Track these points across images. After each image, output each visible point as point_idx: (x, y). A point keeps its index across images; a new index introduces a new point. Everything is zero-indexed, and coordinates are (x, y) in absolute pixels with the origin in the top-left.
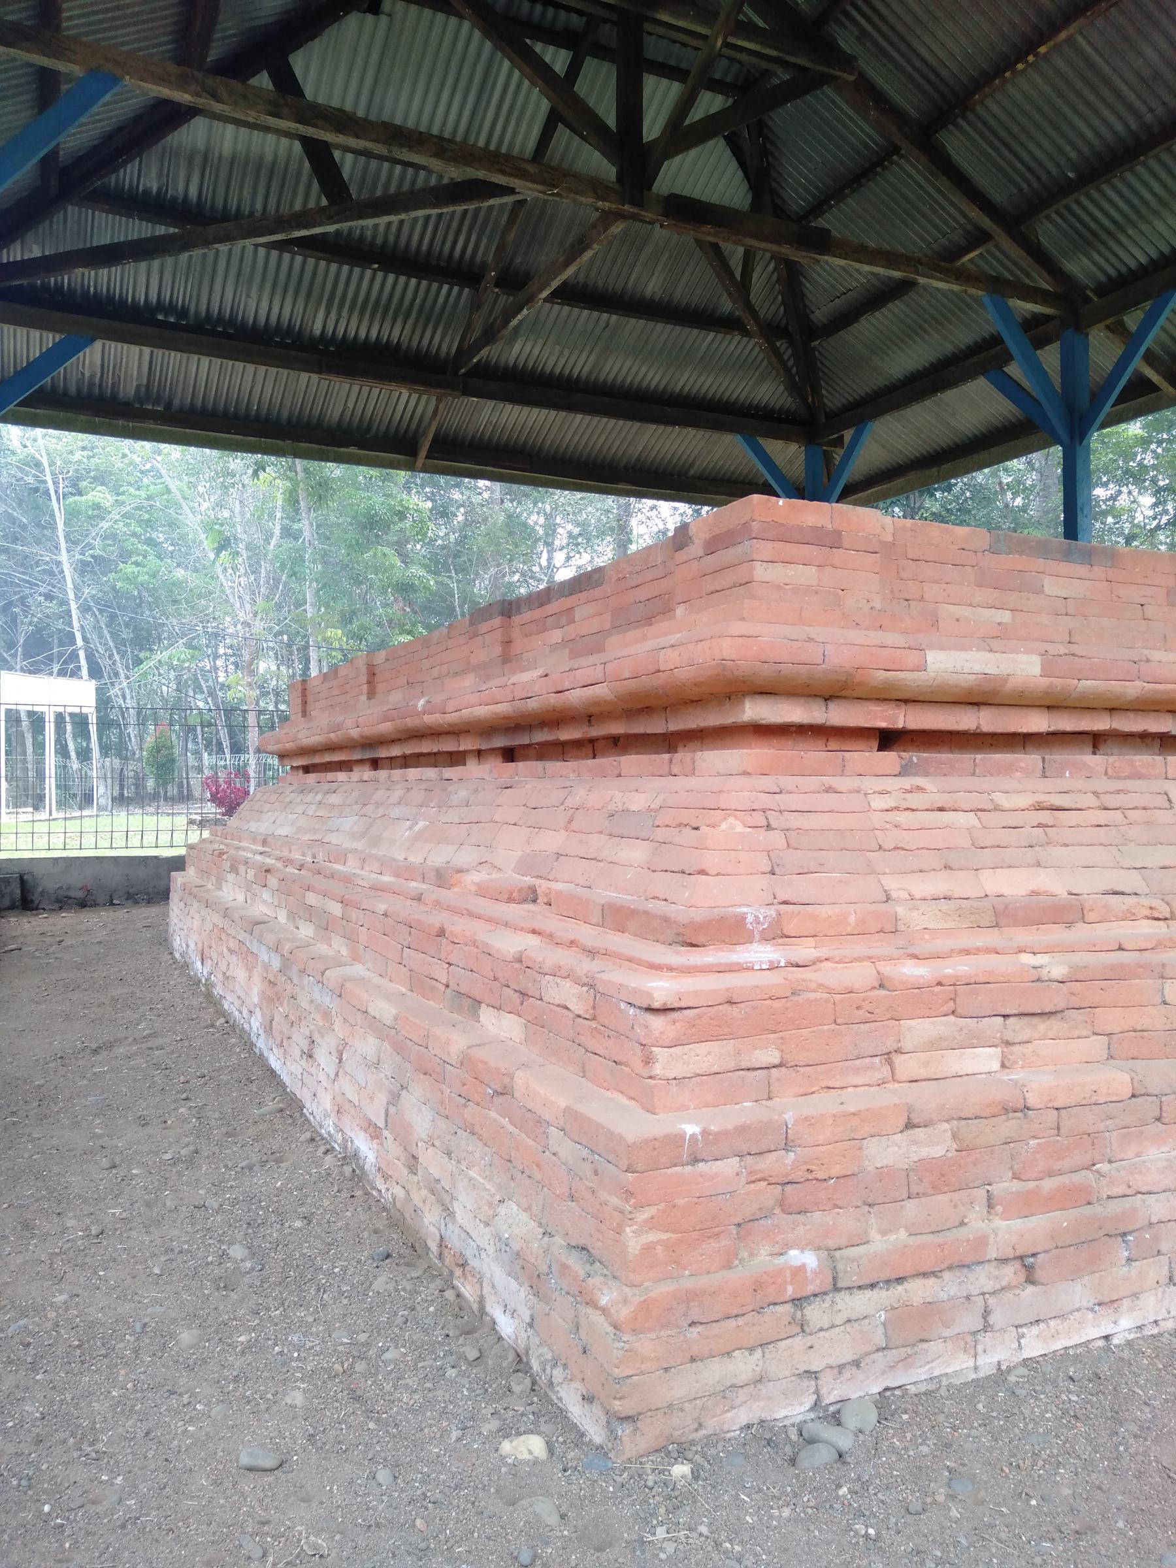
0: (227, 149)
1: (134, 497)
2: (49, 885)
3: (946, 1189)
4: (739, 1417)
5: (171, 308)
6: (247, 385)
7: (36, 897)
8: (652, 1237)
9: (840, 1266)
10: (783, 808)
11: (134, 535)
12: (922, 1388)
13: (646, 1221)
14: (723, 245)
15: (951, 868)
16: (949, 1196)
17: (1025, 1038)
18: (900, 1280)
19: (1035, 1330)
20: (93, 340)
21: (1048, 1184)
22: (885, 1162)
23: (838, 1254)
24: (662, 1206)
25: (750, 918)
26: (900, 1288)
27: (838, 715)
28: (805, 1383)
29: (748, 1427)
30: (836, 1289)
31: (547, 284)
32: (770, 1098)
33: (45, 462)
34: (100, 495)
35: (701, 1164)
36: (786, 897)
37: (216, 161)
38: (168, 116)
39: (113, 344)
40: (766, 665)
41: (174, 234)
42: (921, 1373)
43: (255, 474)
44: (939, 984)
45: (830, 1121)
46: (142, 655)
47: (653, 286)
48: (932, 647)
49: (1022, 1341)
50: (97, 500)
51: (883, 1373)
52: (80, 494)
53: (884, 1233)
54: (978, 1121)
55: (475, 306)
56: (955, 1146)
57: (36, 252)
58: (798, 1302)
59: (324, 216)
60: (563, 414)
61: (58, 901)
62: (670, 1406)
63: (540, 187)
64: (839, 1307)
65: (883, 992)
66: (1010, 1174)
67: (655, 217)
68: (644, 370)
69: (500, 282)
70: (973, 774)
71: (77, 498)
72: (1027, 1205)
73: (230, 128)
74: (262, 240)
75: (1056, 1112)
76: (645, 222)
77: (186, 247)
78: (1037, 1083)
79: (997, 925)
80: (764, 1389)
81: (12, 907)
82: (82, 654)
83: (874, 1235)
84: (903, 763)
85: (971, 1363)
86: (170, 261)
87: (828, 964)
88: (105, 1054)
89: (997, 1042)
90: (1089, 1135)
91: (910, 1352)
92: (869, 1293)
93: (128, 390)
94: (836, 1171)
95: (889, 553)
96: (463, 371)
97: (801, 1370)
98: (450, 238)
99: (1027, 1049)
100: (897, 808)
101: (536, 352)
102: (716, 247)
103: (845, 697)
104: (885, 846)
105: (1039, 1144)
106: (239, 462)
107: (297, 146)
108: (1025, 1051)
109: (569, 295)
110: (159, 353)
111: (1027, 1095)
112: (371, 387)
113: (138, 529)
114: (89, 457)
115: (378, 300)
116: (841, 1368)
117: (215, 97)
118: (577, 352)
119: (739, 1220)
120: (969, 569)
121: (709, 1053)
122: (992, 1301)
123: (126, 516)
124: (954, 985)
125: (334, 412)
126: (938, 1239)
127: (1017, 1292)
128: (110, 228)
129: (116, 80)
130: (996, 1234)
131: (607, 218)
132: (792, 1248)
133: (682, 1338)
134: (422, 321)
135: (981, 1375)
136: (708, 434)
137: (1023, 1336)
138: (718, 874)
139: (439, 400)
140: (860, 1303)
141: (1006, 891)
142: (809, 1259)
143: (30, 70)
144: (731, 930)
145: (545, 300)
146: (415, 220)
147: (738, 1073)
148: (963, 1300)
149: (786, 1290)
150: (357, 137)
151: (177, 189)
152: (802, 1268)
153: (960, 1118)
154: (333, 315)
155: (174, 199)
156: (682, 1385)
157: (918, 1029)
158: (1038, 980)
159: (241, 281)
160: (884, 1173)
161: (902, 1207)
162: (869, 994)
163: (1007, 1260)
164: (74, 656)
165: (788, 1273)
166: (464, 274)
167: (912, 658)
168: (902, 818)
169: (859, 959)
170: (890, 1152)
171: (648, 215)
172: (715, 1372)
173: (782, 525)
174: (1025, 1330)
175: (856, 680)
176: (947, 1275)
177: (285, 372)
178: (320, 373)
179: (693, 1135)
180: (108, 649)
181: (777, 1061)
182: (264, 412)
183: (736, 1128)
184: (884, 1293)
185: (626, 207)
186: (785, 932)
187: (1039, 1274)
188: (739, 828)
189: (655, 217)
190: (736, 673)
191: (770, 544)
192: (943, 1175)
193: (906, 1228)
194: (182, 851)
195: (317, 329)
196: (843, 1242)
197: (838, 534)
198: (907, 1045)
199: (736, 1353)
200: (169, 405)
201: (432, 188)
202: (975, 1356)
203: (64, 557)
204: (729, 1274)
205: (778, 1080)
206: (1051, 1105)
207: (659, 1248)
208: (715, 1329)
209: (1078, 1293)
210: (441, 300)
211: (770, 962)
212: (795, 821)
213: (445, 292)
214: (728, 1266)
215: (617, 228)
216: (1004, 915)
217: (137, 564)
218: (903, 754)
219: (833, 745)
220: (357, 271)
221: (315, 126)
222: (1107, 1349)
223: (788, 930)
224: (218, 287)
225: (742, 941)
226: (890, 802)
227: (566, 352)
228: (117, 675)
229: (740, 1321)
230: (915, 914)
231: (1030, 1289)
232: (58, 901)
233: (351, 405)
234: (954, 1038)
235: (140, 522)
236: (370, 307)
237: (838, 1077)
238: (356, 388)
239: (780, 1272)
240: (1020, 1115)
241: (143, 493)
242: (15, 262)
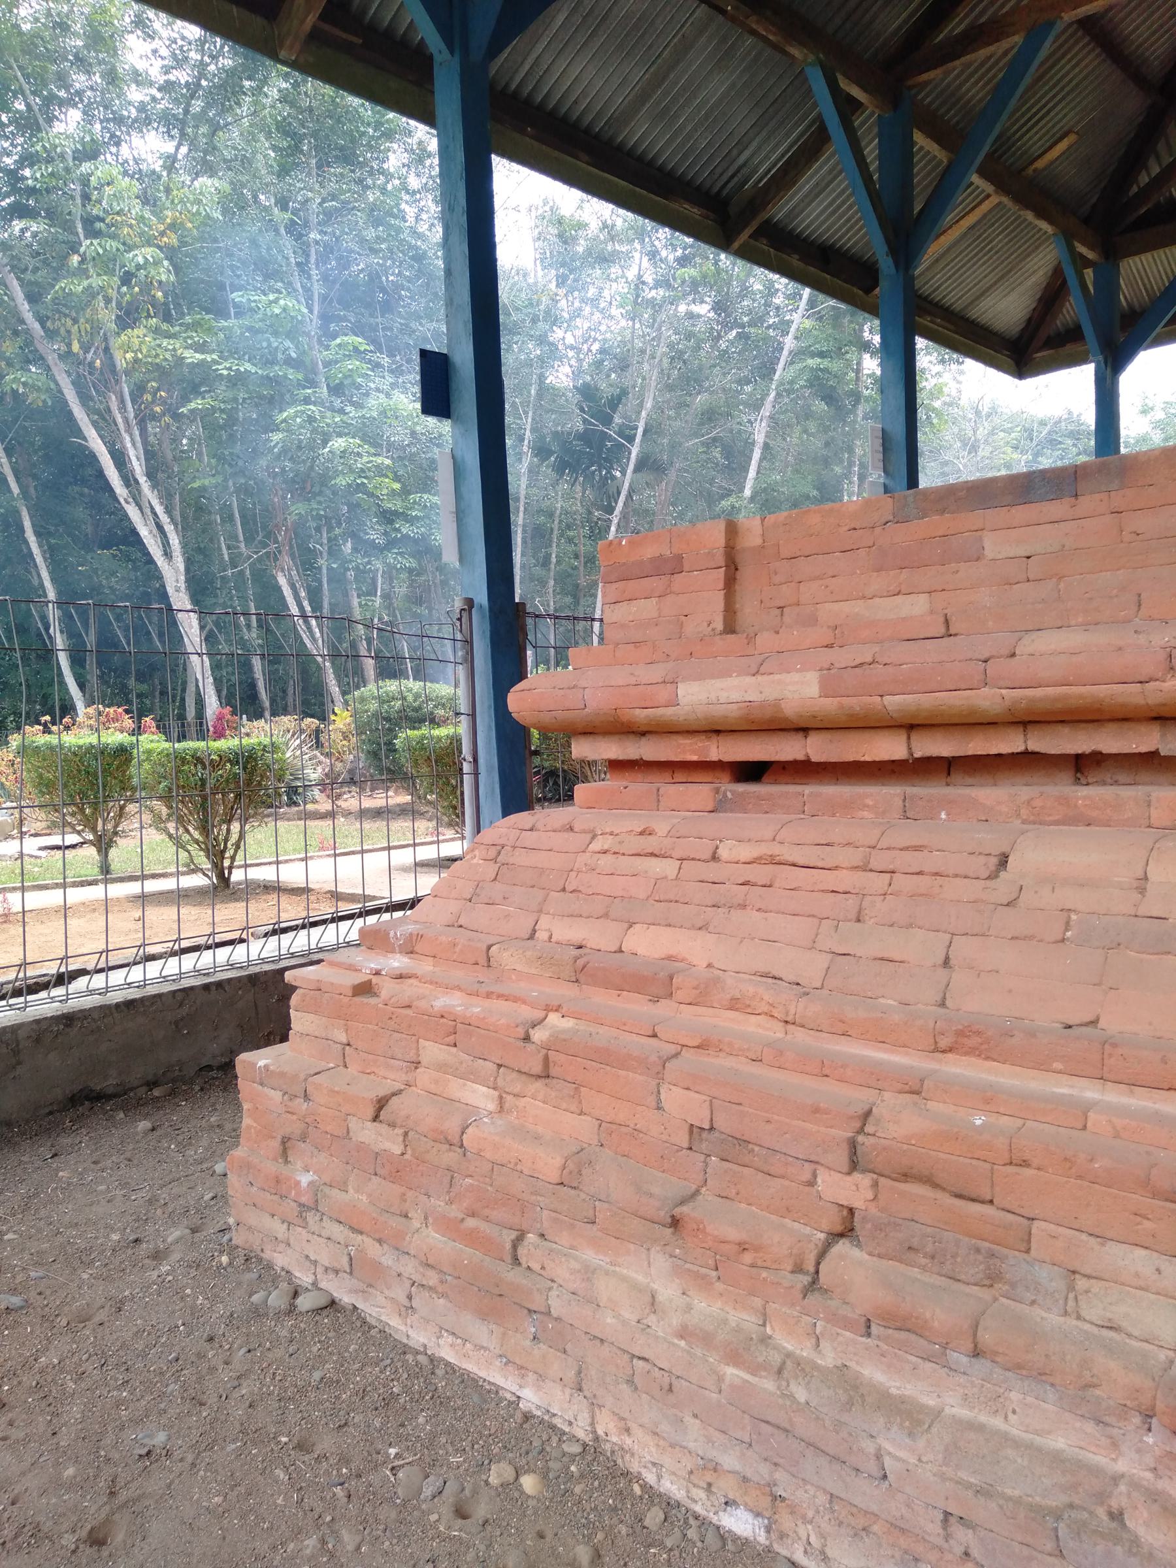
79: (577, 981)
105: (471, 1185)
127: (434, 1296)
162: (400, 1010)
167: (663, 694)
197: (679, 558)
219: (679, 777)
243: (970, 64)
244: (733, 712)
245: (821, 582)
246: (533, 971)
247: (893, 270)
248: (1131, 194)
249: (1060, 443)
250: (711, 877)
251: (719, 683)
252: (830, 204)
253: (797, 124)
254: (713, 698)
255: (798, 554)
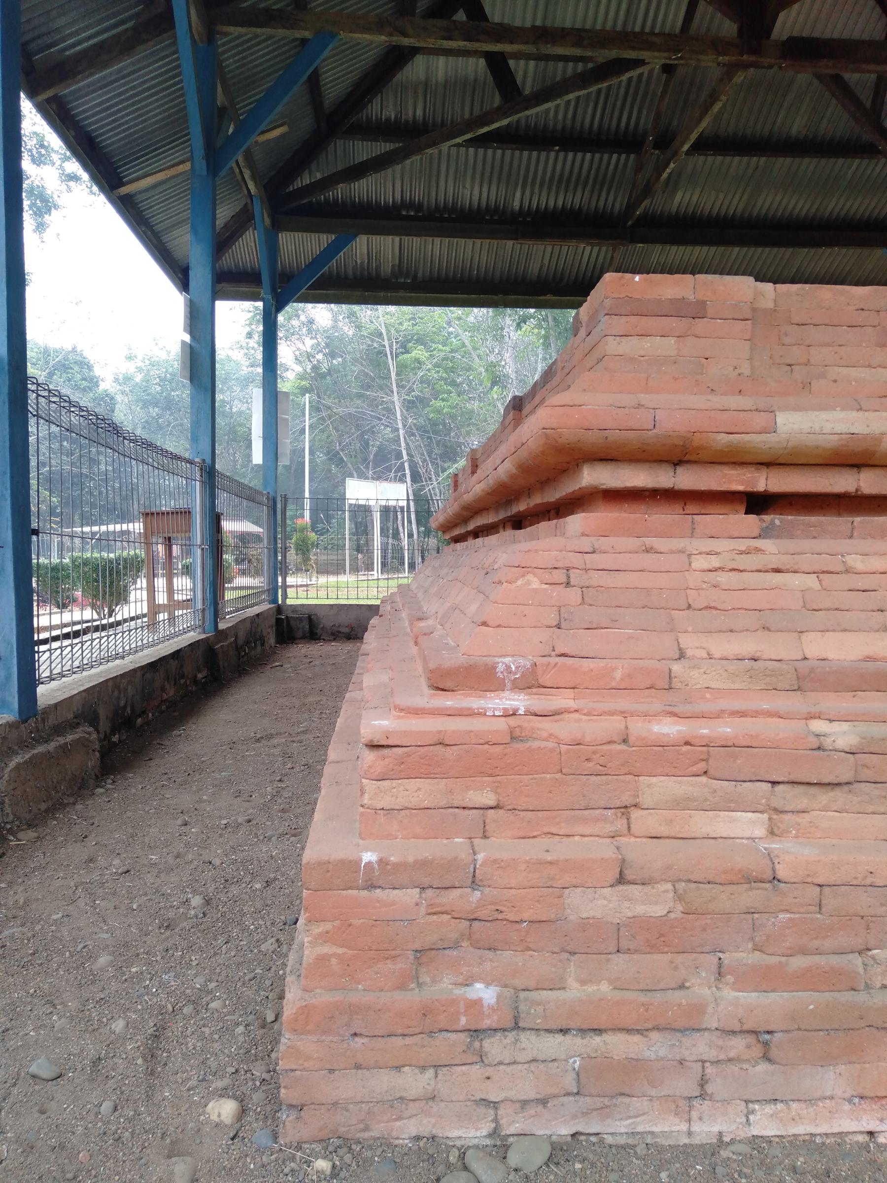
0: (441, 75)
1: (441, 351)
2: (327, 623)
3: (666, 949)
4: (407, 1129)
5: (411, 205)
6: (437, 253)
7: (319, 631)
8: (326, 949)
9: (522, 1007)
10: (588, 566)
11: (442, 379)
12: (622, 1141)
13: (320, 935)
14: (847, 76)
15: (769, 630)
16: (669, 956)
17: (800, 807)
18: (598, 1031)
19: (769, 1109)
20: (356, 236)
21: (798, 962)
22: (591, 914)
23: (522, 995)
24: (337, 923)
25: (501, 667)
26: (598, 1039)
27: (686, 479)
28: (482, 1110)
29: (417, 1138)
30: (517, 1027)
31: (687, 138)
32: (485, 837)
33: (384, 331)
34: (419, 352)
35: (378, 891)
36: (565, 650)
37: (433, 87)
38: (396, 59)
39: (374, 237)
40: (590, 432)
41: (400, 147)
42: (622, 1127)
43: (519, 327)
44: (687, 743)
45: (523, 867)
46: (446, 465)
47: (797, 126)
48: (785, 408)
49: (751, 1117)
50: (417, 356)
51: (574, 1117)
52: (407, 352)
53: (583, 983)
54: (711, 886)
55: (639, 168)
56: (681, 909)
57: (319, 176)
58: (476, 1033)
59: (501, 112)
60: (721, 249)
61: (333, 634)
62: (334, 1104)
63: (665, 55)
64: (523, 1045)
65: (623, 747)
66: (750, 945)
67: (773, 61)
68: (793, 201)
69: (657, 145)
70: (851, 537)
71: (405, 356)
72: (765, 979)
73: (442, 60)
74: (459, 140)
75: (818, 889)
76: (764, 67)
77: (407, 156)
78: (794, 854)
79: (799, 689)
80: (435, 1108)
81: (304, 637)
82: (406, 465)
83: (572, 982)
84: (764, 525)
85: (684, 1127)
86: (398, 167)
87: (575, 716)
88: (264, 742)
89: (762, 808)
90: (862, 917)
91: (606, 1103)
92: (559, 1038)
93: (387, 269)
94: (527, 915)
95: (754, 316)
96: (630, 223)
97: (478, 1098)
98: (616, 114)
99: (805, 819)
100: (721, 569)
101: (695, 199)
102: (838, 80)
103: (696, 462)
104: (694, 605)
105: (790, 919)
106: (509, 317)
107: (482, 62)
108: (800, 820)
109: (703, 146)
110: (406, 239)
111: (777, 866)
112: (561, 246)
113: (444, 375)
114: (414, 325)
115: (562, 175)
116: (524, 1104)
117: (404, 34)
118: (730, 196)
119: (417, 946)
120: (869, 330)
121: (419, 789)
122: (710, 1070)
123: (436, 366)
124: (707, 746)
125: (534, 269)
126: (643, 998)
127: (745, 1066)
128: (364, 150)
129: (333, 35)
130: (717, 1005)
131: (731, 69)
132: (476, 981)
133: (345, 1046)
134: (597, 187)
135: (696, 1141)
136: (859, 250)
137: (753, 1112)
138: (499, 626)
139: (614, 250)
140: (551, 1045)
141: (830, 656)
142: (485, 993)
143: (298, 42)
144: (483, 678)
145: (688, 153)
146: (568, 102)
147: (451, 810)
148: (675, 1063)
149: (459, 1020)
150: (512, 43)
151: (408, 114)
152: (478, 1002)
153: (689, 881)
154: (528, 193)
155: (407, 122)
156: (347, 1087)
157: (660, 787)
158: (819, 748)
159: (458, 175)
160: (585, 924)
161: (608, 960)
163: (734, 1032)
164: (401, 468)
165: (462, 1004)
166: (627, 142)
167: (760, 420)
168: (723, 578)
169: (612, 713)
170: (602, 904)
171: (766, 61)
172: (382, 1082)
173: (638, 300)
174: (757, 1107)
175: (695, 444)
176: (654, 1035)
177: (496, 242)
178: (516, 239)
179: (369, 864)
180: (425, 460)
181: (492, 803)
182: (483, 275)
183: (416, 862)
184: (578, 1041)
185: (745, 57)
186: (540, 681)
187: (774, 1053)
188: (535, 584)
189: (773, 61)
190: (560, 440)
191: (623, 319)
192: (662, 935)
193: (610, 981)
194: (378, 602)
195: (516, 204)
196: (531, 984)
197: (702, 304)
198: (646, 799)
199: (406, 1069)
200: (415, 277)
201: (580, 74)
202: (689, 1121)
203: (396, 398)
204: (398, 995)
205: (494, 821)
206: (809, 880)
207: (334, 961)
208: (381, 1043)
209: (833, 1081)
210: (612, 167)
211: (504, 709)
212: (596, 578)
213: (614, 161)
214: (402, 987)
215: (740, 78)
216: (809, 679)
217: (443, 400)
218: (765, 517)
219: (691, 508)
220: (544, 154)
221: (478, 41)
222: (865, 1147)
223: (545, 680)
224: (442, 184)
225: (491, 688)
226: (715, 562)
227: (721, 196)
228: (430, 479)
229: (408, 1041)
230: (695, 673)
231: (763, 1067)
232: (333, 634)
233: (546, 262)
234: (706, 800)
235: (446, 370)
236: (555, 183)
237: (563, 825)
238: (549, 248)
239: (454, 1002)
240: (767, 885)
241: (448, 349)
242: (307, 185)
243: (256, 36)
244: (829, 441)
245: (831, 348)
246: (737, 686)
247: (205, 173)
248: (287, 191)
249: (71, 368)
250: (861, 586)
251: (824, 415)
252: (107, 100)
253: (109, 18)
254: (817, 428)
255: (809, 321)
